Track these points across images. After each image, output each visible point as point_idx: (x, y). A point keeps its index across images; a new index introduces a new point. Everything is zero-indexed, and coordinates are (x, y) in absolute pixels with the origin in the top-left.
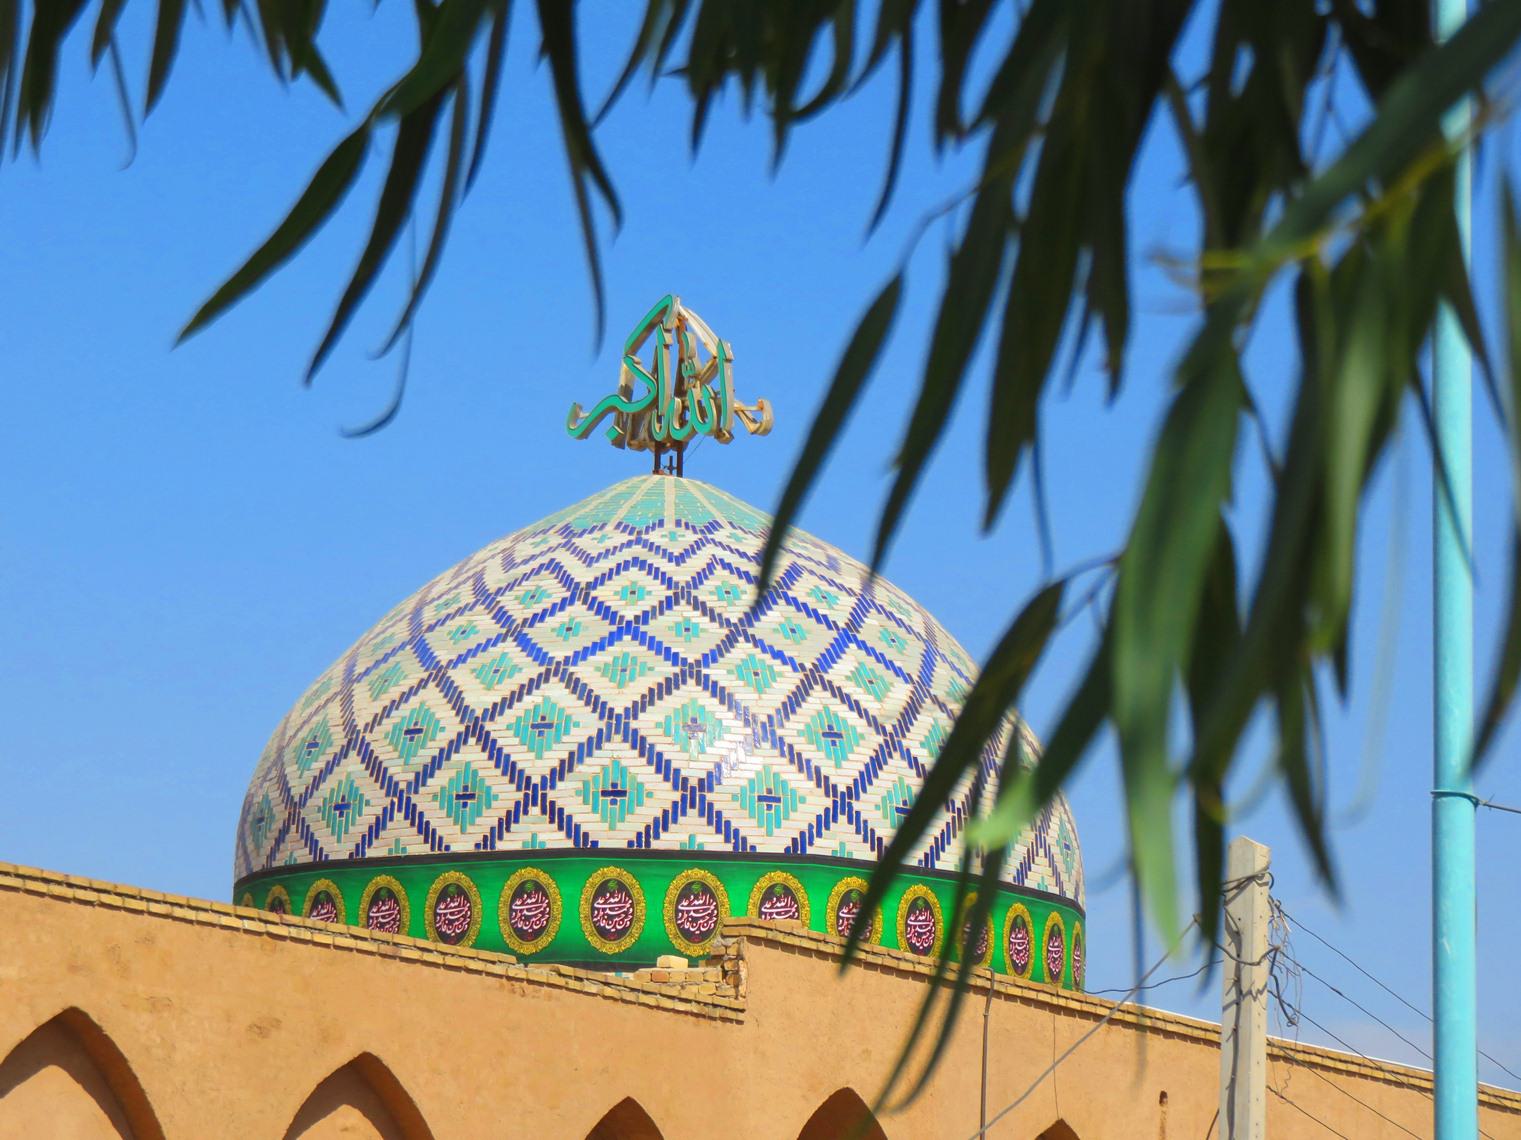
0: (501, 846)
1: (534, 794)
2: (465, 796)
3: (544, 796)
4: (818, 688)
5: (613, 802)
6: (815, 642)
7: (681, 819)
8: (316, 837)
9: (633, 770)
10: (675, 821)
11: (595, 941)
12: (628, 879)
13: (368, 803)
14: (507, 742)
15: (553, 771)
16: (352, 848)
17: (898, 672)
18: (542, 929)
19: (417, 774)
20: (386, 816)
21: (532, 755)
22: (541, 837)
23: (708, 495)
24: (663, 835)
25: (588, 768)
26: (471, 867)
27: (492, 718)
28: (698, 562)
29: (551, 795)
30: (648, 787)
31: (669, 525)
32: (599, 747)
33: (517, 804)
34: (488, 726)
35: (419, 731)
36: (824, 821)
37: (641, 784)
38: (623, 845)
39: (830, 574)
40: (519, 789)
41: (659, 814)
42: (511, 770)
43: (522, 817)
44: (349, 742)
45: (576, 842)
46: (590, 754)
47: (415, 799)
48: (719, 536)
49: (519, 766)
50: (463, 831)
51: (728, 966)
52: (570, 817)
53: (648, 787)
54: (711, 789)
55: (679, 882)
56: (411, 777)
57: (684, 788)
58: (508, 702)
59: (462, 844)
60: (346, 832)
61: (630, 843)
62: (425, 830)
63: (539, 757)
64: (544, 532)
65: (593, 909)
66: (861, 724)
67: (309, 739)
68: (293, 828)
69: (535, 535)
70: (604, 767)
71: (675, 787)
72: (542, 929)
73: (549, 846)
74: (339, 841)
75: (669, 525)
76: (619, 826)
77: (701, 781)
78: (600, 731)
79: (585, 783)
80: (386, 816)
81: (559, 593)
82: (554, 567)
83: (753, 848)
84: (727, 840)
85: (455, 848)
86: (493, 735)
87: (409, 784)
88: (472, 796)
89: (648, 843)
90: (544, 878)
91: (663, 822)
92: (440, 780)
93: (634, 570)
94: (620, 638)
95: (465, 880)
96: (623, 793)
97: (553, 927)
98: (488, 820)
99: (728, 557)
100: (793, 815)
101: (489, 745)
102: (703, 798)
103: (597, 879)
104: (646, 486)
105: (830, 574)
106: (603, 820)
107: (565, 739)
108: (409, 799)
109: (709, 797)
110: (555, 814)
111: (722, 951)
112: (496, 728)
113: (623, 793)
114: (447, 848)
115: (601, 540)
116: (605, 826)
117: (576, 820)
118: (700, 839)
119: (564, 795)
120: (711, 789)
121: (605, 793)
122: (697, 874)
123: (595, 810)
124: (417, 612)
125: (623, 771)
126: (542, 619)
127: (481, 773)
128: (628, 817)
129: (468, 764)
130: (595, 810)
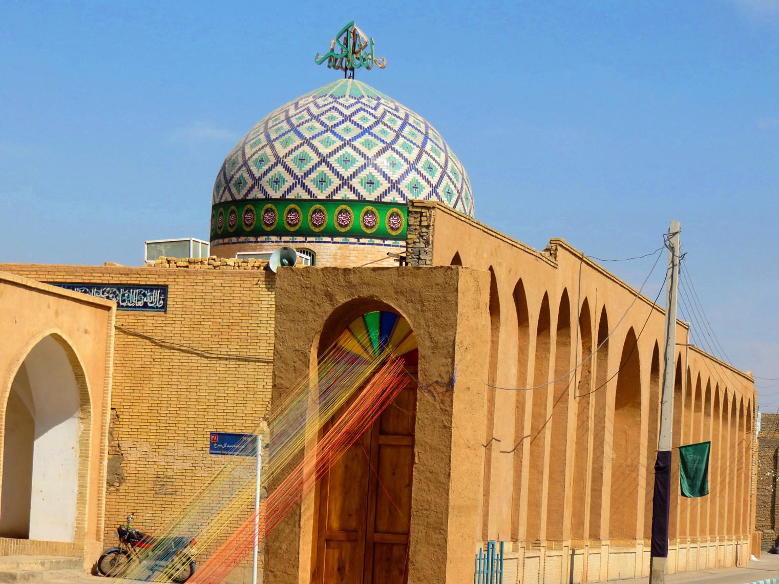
0: (334, 198)
1: (345, 182)
2: (322, 181)
3: (348, 183)
4: (390, 149)
5: (370, 186)
6: (390, 137)
7: (391, 192)
8: (266, 190)
9: (376, 176)
10: (389, 193)
11: (364, 229)
12: (374, 210)
13: (287, 181)
14: (336, 165)
15: (351, 175)
16: (281, 195)
17: (414, 144)
18: (348, 224)
19: (305, 173)
20: (294, 185)
21: (344, 170)
22: (348, 196)
23: (363, 87)
24: (385, 197)
25: (362, 175)
26: (324, 204)
27: (329, 157)
28: (353, 109)
29: (351, 183)
30: (381, 182)
31: (347, 97)
32: (365, 168)
33: (340, 185)
34: (329, 160)
35: (304, 160)
36: (430, 195)
37: (379, 181)
38: (373, 200)
39: (395, 113)
40: (340, 180)
41: (384, 190)
42: (338, 174)
43: (341, 189)
44: (277, 161)
45: (359, 198)
46: (362, 171)
47: (304, 181)
48: (363, 100)
49: (340, 173)
50: (322, 192)
51: (552, 252)
52: (357, 190)
53: (381, 182)
54: (399, 184)
55: (390, 212)
56: (303, 174)
57: (392, 183)
58: (291, 152)
59: (322, 196)
60: (279, 190)
61: (376, 199)
62: (309, 191)
63: (346, 170)
64: (308, 97)
65: (364, 219)
66: (402, 161)
67: (260, 159)
68: (256, 187)
69: (305, 98)
70: (367, 175)
71: (389, 182)
72: (348, 224)
73: (350, 199)
74: (276, 192)
75: (347, 97)
76: (372, 194)
77: (396, 181)
78: (365, 164)
79: (362, 180)
80: (294, 185)
81: (308, 117)
82: (308, 110)
83: (365, 199)
84: (404, 200)
85: (318, 197)
86: (330, 163)
87: (302, 176)
88: (325, 181)
89: (381, 199)
90: (348, 208)
91: (386, 193)
92: (313, 176)
93: (362, 112)
94: (365, 134)
95: (322, 208)
96: (373, 183)
97: (351, 224)
98: (330, 189)
99: (389, 110)
100: (422, 193)
101: (329, 165)
102: (397, 186)
103: (365, 209)
104: (342, 83)
105: (395, 113)
106: (367, 191)
107: (354, 165)
108: (302, 181)
109: (399, 186)
110: (352, 189)
111: (550, 247)
112: (331, 160)
113: (373, 183)
114: (316, 197)
115: (324, 101)
116: (368, 193)
117: (359, 191)
118: (396, 199)
119: (355, 182)
120: (399, 184)
121: (368, 183)
122: (395, 210)
123: (365, 188)
124: (267, 123)
125: (373, 176)
126: (302, 125)
127: (327, 174)
128: (375, 191)
129: (323, 171)
130: (365, 188)
